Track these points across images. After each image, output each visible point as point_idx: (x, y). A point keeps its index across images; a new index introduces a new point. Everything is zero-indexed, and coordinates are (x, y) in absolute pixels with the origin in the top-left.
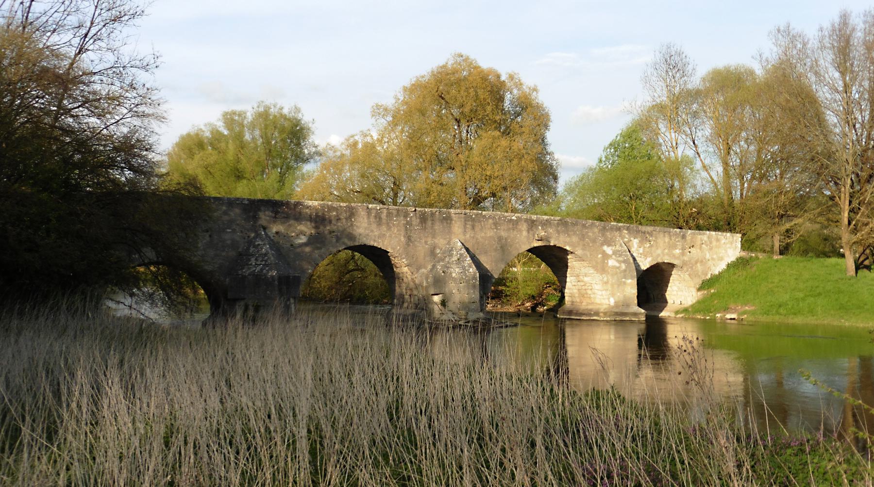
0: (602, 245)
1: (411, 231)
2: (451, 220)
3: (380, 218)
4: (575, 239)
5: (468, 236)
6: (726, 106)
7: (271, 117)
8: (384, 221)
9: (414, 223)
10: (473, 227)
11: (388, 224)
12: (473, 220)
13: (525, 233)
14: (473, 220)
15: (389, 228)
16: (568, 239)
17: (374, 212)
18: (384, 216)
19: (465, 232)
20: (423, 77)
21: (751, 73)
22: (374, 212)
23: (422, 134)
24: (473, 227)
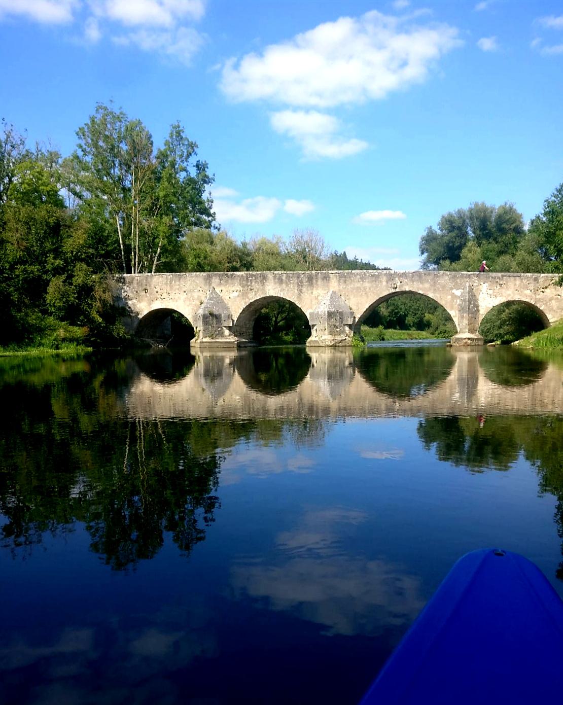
0: (452, 289)
1: (302, 286)
2: (329, 278)
3: (282, 280)
4: (427, 285)
5: (341, 287)
6: (51, 336)
7: (205, 488)
8: (284, 281)
9: (304, 281)
10: (345, 282)
11: (286, 283)
12: (345, 277)
13: (384, 283)
14: (345, 277)
15: (287, 285)
16: (421, 286)
17: (278, 276)
18: (284, 278)
19: (339, 285)
20: (559, 531)
21: (439, 447)
22: (278, 276)
23: (59, 157)
24: (345, 282)
